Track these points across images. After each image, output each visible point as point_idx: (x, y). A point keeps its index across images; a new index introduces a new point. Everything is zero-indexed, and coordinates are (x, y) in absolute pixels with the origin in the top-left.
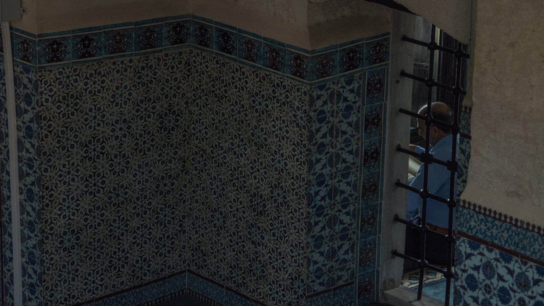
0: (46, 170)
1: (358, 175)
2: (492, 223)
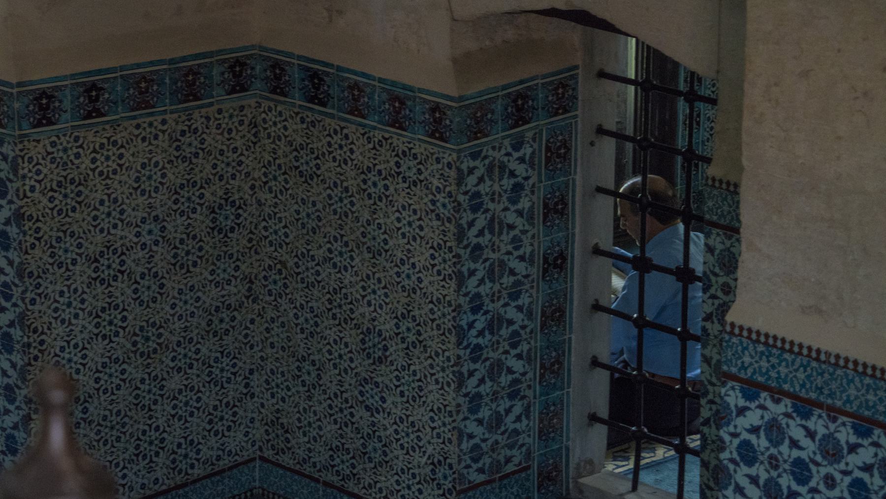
0: (33, 302)
1: (534, 295)
2: (778, 357)
